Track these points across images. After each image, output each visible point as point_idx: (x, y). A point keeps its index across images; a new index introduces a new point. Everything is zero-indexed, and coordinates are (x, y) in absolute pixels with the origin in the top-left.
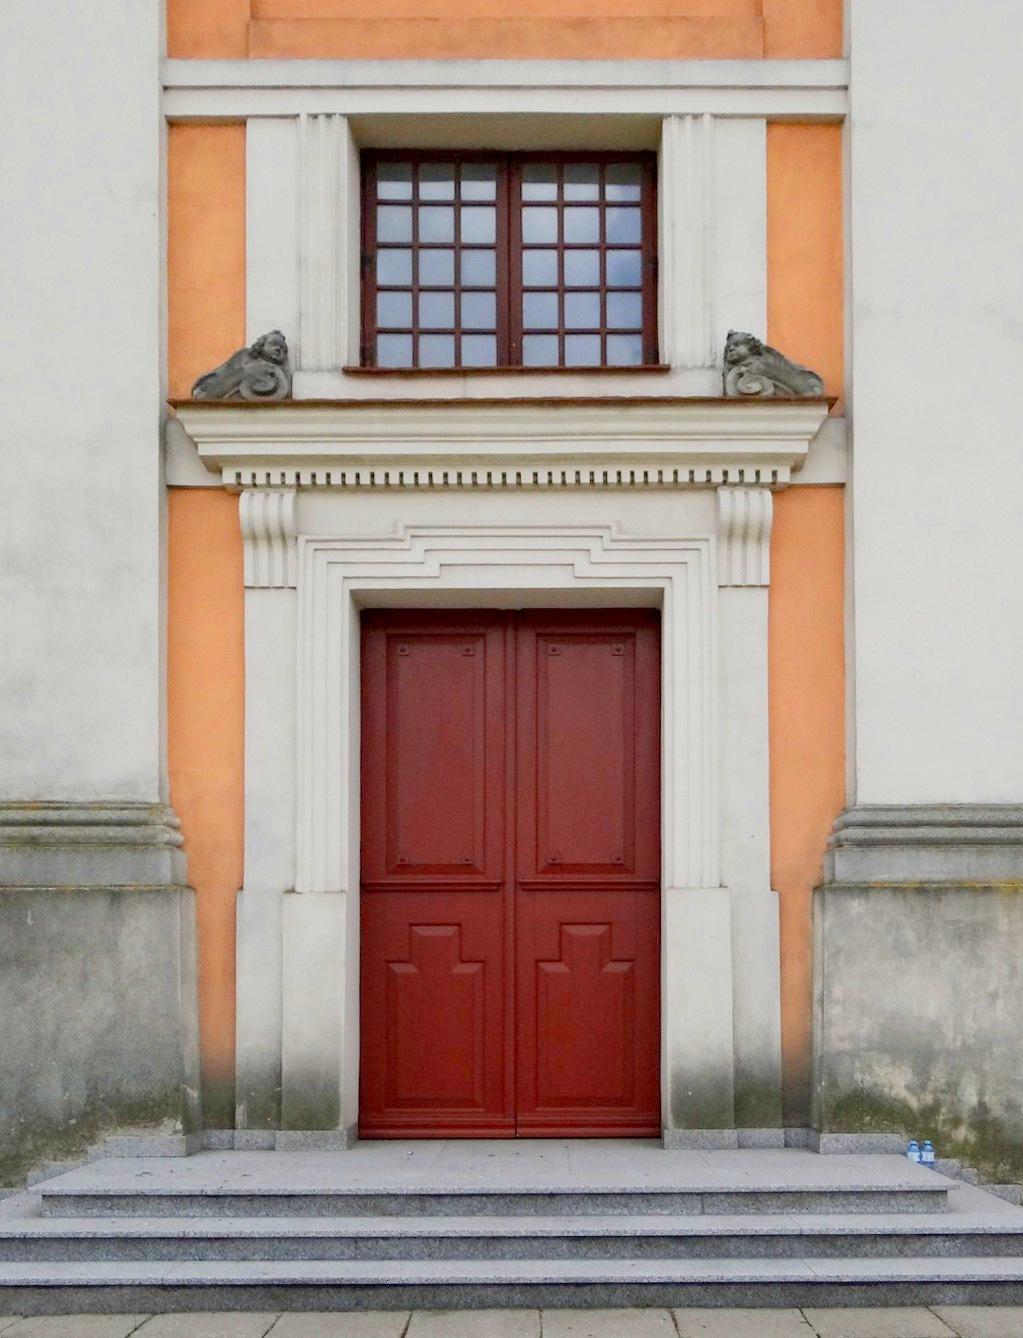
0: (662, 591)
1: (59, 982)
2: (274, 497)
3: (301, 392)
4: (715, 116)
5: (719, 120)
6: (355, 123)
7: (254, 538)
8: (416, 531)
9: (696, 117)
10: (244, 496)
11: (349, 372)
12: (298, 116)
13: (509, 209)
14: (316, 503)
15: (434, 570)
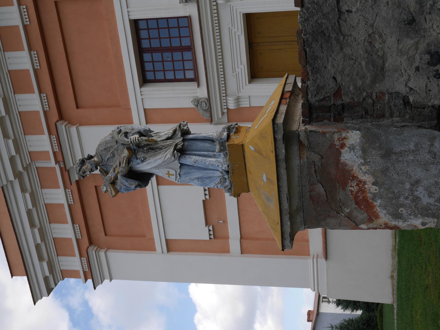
0: (243, 14)
1: (228, 172)
2: (229, 101)
3: (206, 96)
4: (127, 8)
5: (128, 6)
6: (141, 86)
7: (239, 105)
8: (234, 70)
9: (128, 12)
10: (230, 108)
11: (199, 86)
12: (142, 99)
13: (152, 50)
14: (229, 92)
15: (242, 66)
